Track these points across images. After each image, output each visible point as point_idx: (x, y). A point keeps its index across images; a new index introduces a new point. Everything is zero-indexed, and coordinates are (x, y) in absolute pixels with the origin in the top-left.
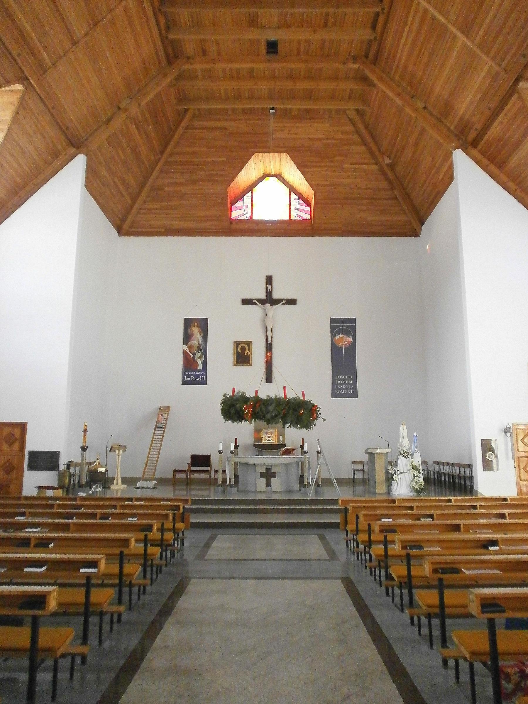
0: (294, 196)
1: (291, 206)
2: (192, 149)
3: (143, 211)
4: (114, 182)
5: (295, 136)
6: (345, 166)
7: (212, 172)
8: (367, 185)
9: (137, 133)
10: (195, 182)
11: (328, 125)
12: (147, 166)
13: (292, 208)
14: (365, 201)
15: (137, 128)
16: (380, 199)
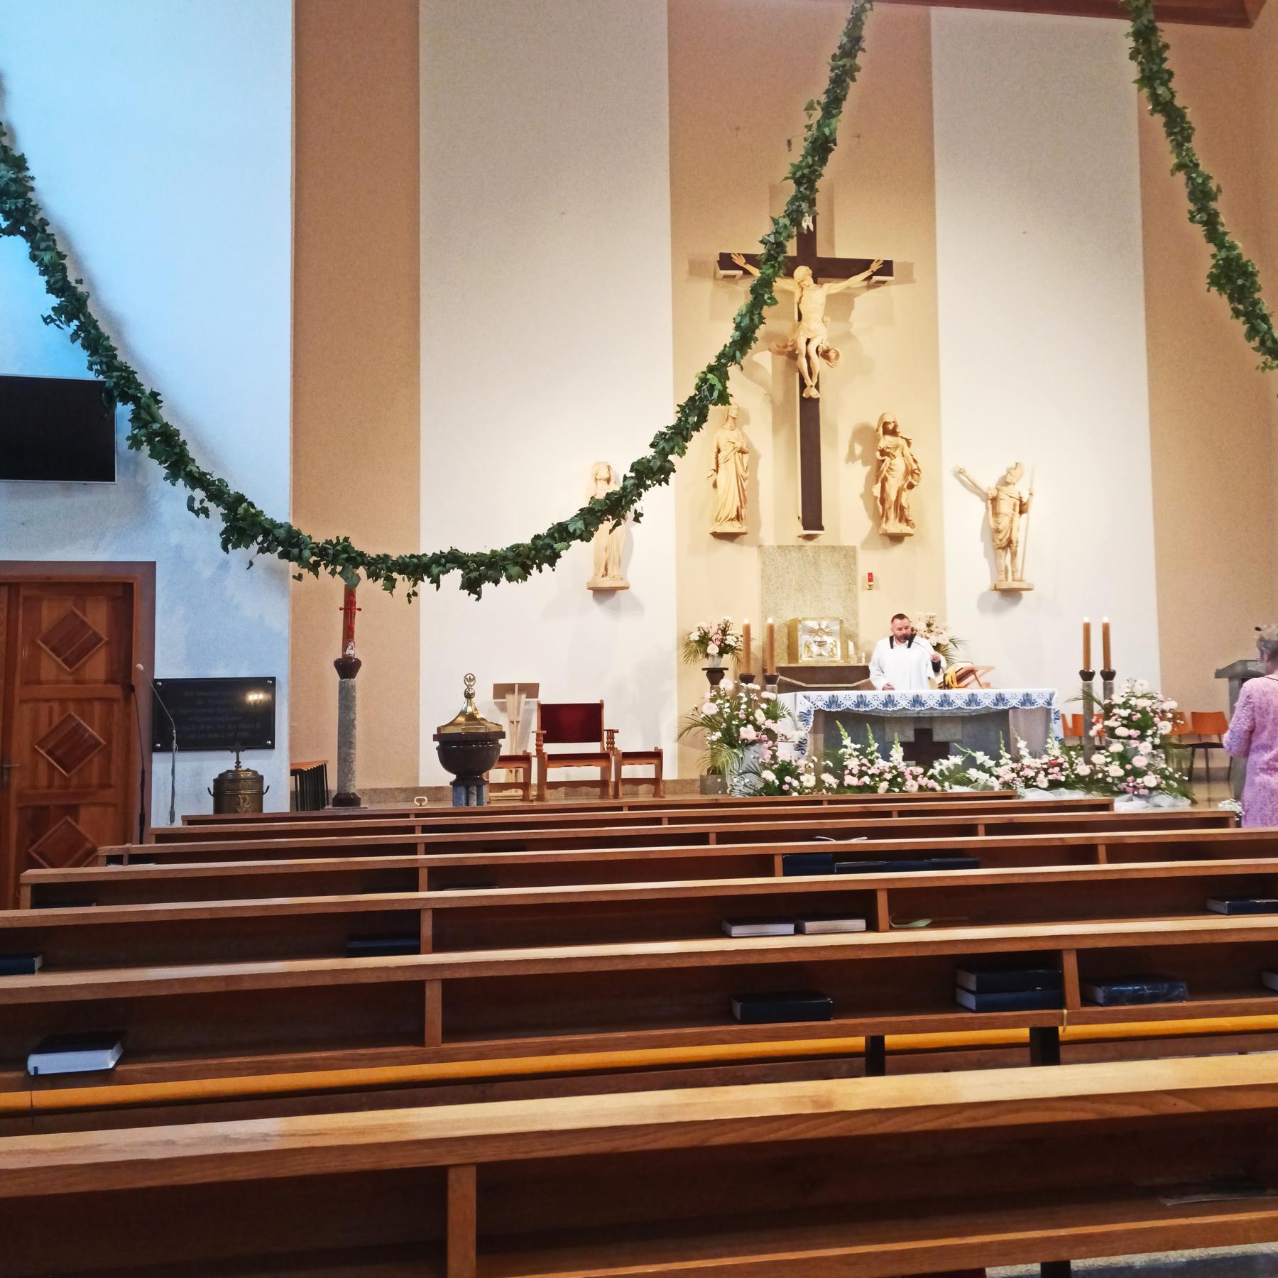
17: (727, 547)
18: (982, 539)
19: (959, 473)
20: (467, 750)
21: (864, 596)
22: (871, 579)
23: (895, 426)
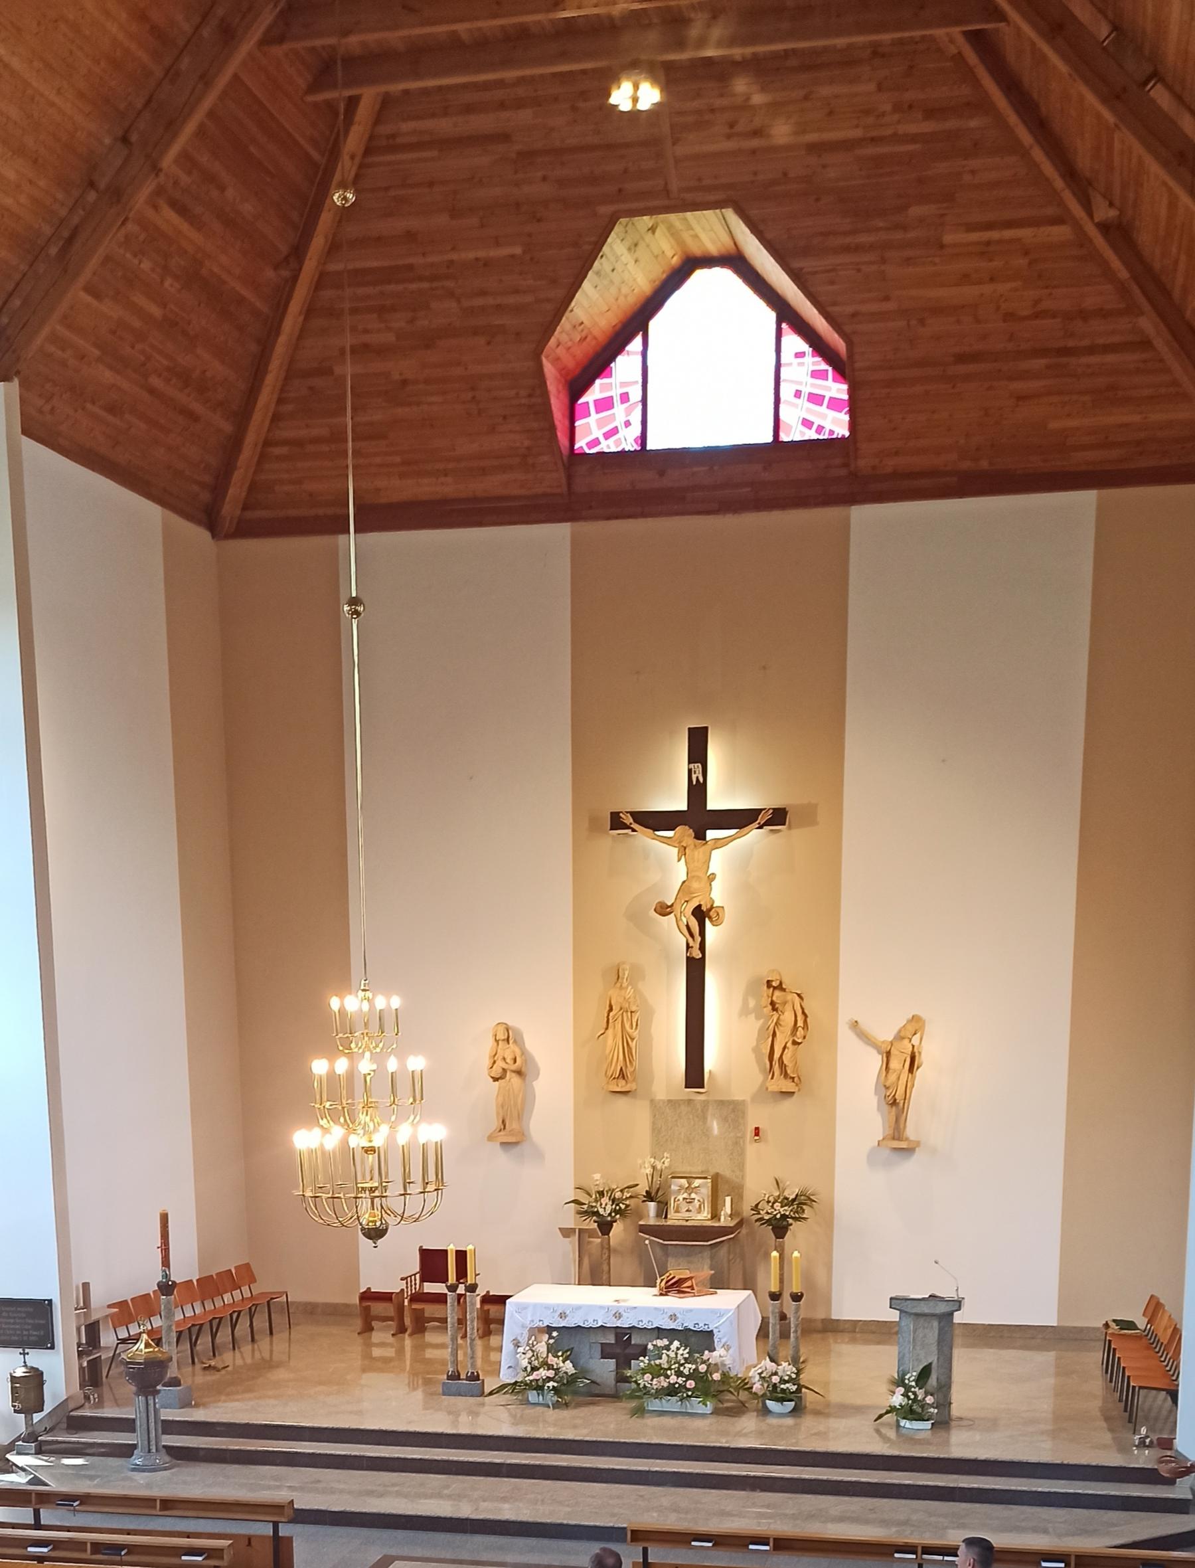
0: (793, 343)
1: (783, 386)
2: (398, 225)
3: (277, 451)
4: (152, 391)
5: (755, 143)
6: (948, 238)
7: (479, 302)
8: (1037, 302)
9: (185, 227)
10: (428, 340)
11: (872, 87)
12: (258, 304)
13: (786, 392)
14: (1039, 363)
15: (182, 210)
16: (1091, 350)
17: (622, 1101)
18: (876, 1093)
19: (855, 1025)
20: (756, 1208)
21: (752, 1149)
22: (757, 1134)
23: (781, 983)
